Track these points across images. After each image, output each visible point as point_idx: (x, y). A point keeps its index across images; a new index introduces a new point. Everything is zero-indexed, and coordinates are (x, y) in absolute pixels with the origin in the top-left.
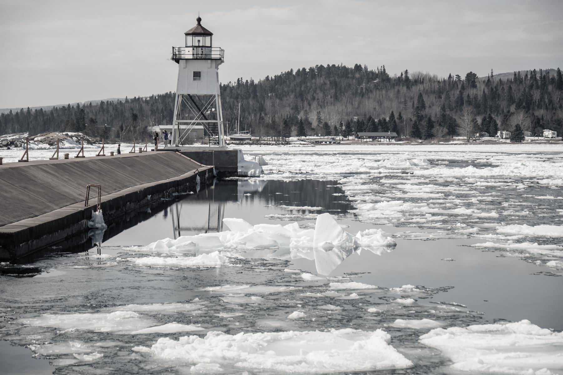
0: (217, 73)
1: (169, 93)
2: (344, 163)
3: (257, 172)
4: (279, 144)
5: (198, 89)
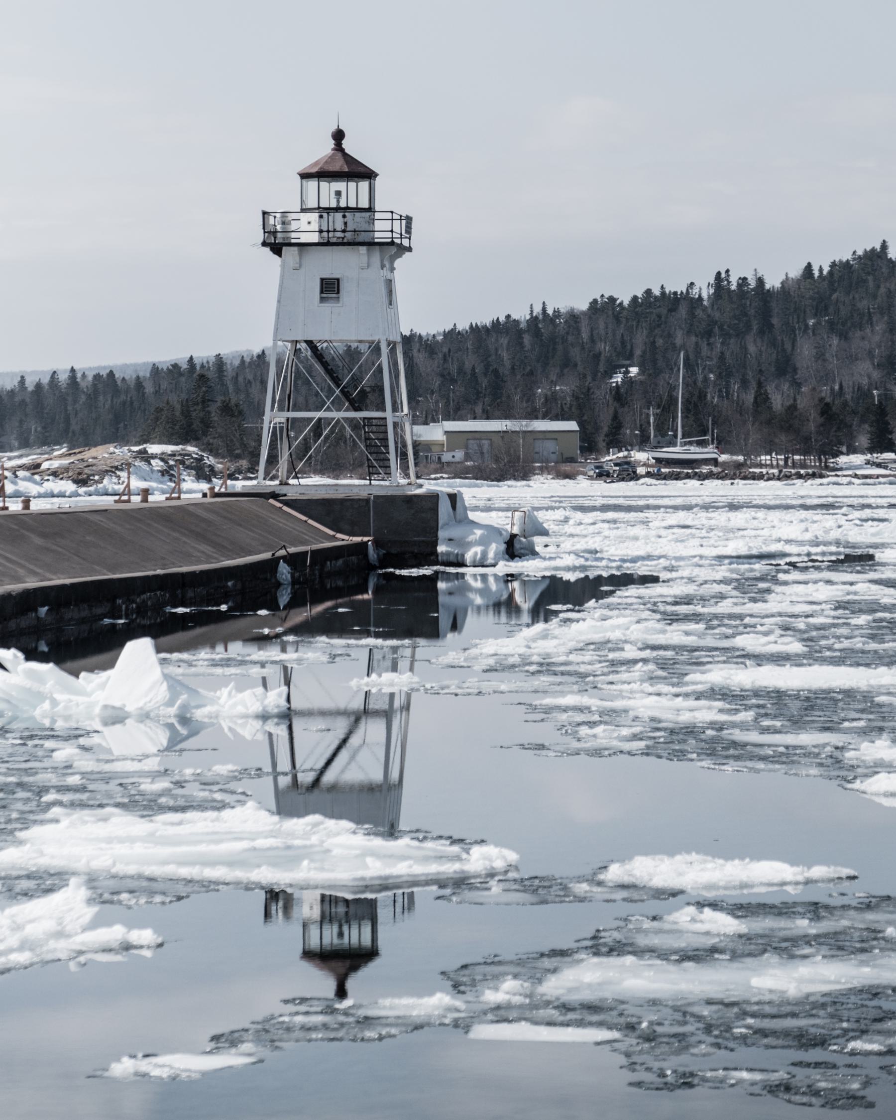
0: (389, 283)
1: (502, 319)
2: (873, 530)
3: (491, 555)
4: (788, 477)
5: (339, 327)
